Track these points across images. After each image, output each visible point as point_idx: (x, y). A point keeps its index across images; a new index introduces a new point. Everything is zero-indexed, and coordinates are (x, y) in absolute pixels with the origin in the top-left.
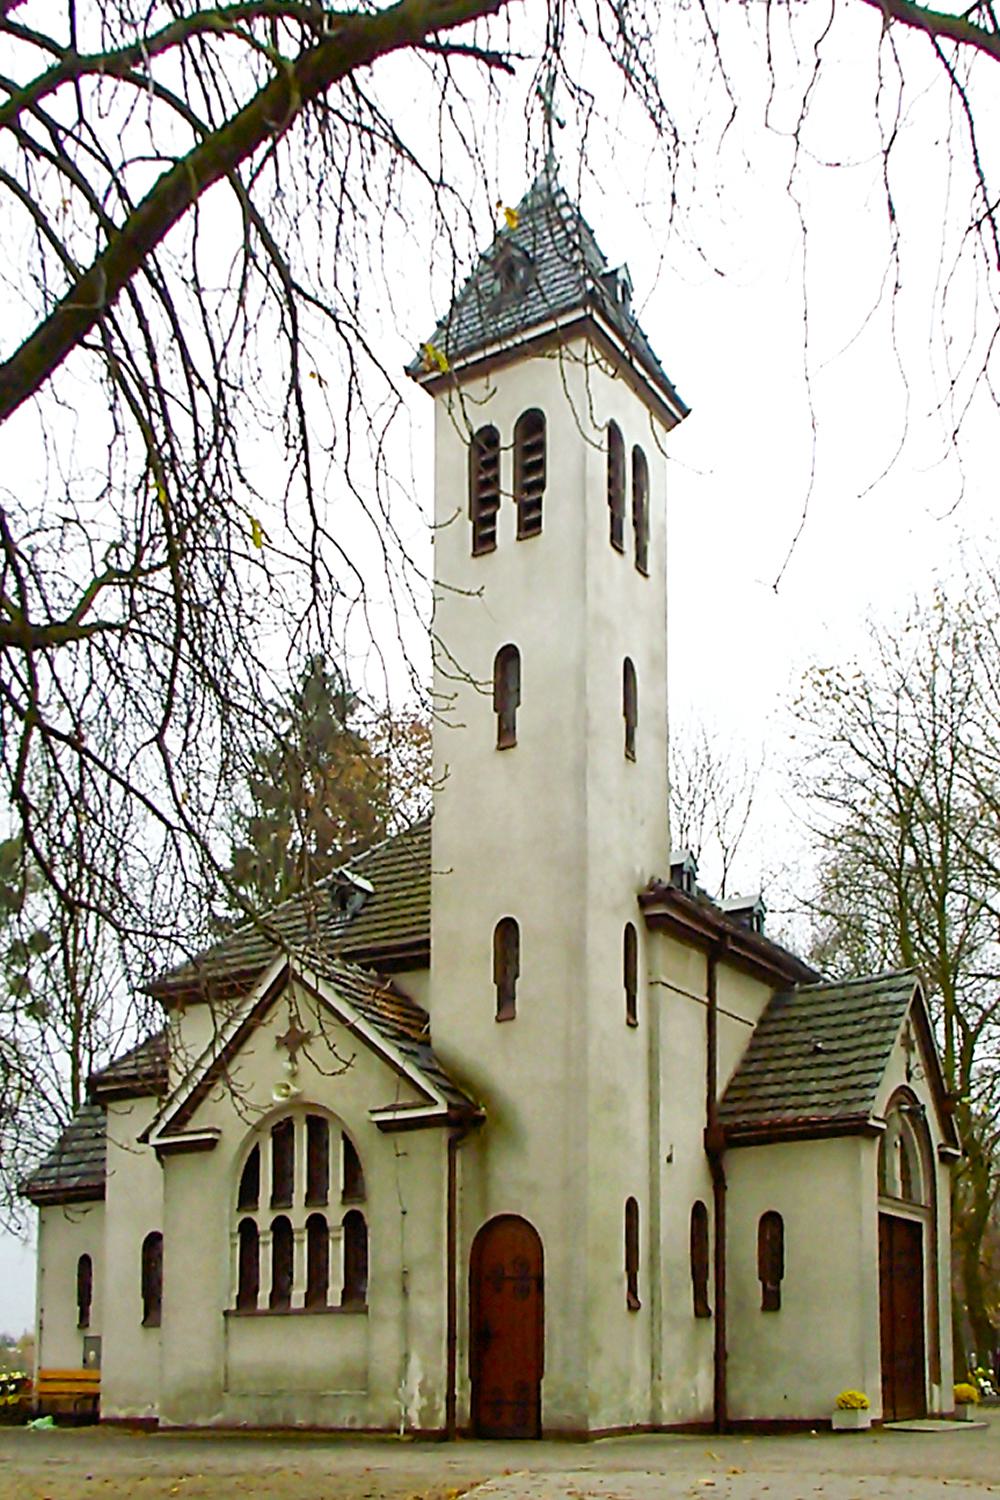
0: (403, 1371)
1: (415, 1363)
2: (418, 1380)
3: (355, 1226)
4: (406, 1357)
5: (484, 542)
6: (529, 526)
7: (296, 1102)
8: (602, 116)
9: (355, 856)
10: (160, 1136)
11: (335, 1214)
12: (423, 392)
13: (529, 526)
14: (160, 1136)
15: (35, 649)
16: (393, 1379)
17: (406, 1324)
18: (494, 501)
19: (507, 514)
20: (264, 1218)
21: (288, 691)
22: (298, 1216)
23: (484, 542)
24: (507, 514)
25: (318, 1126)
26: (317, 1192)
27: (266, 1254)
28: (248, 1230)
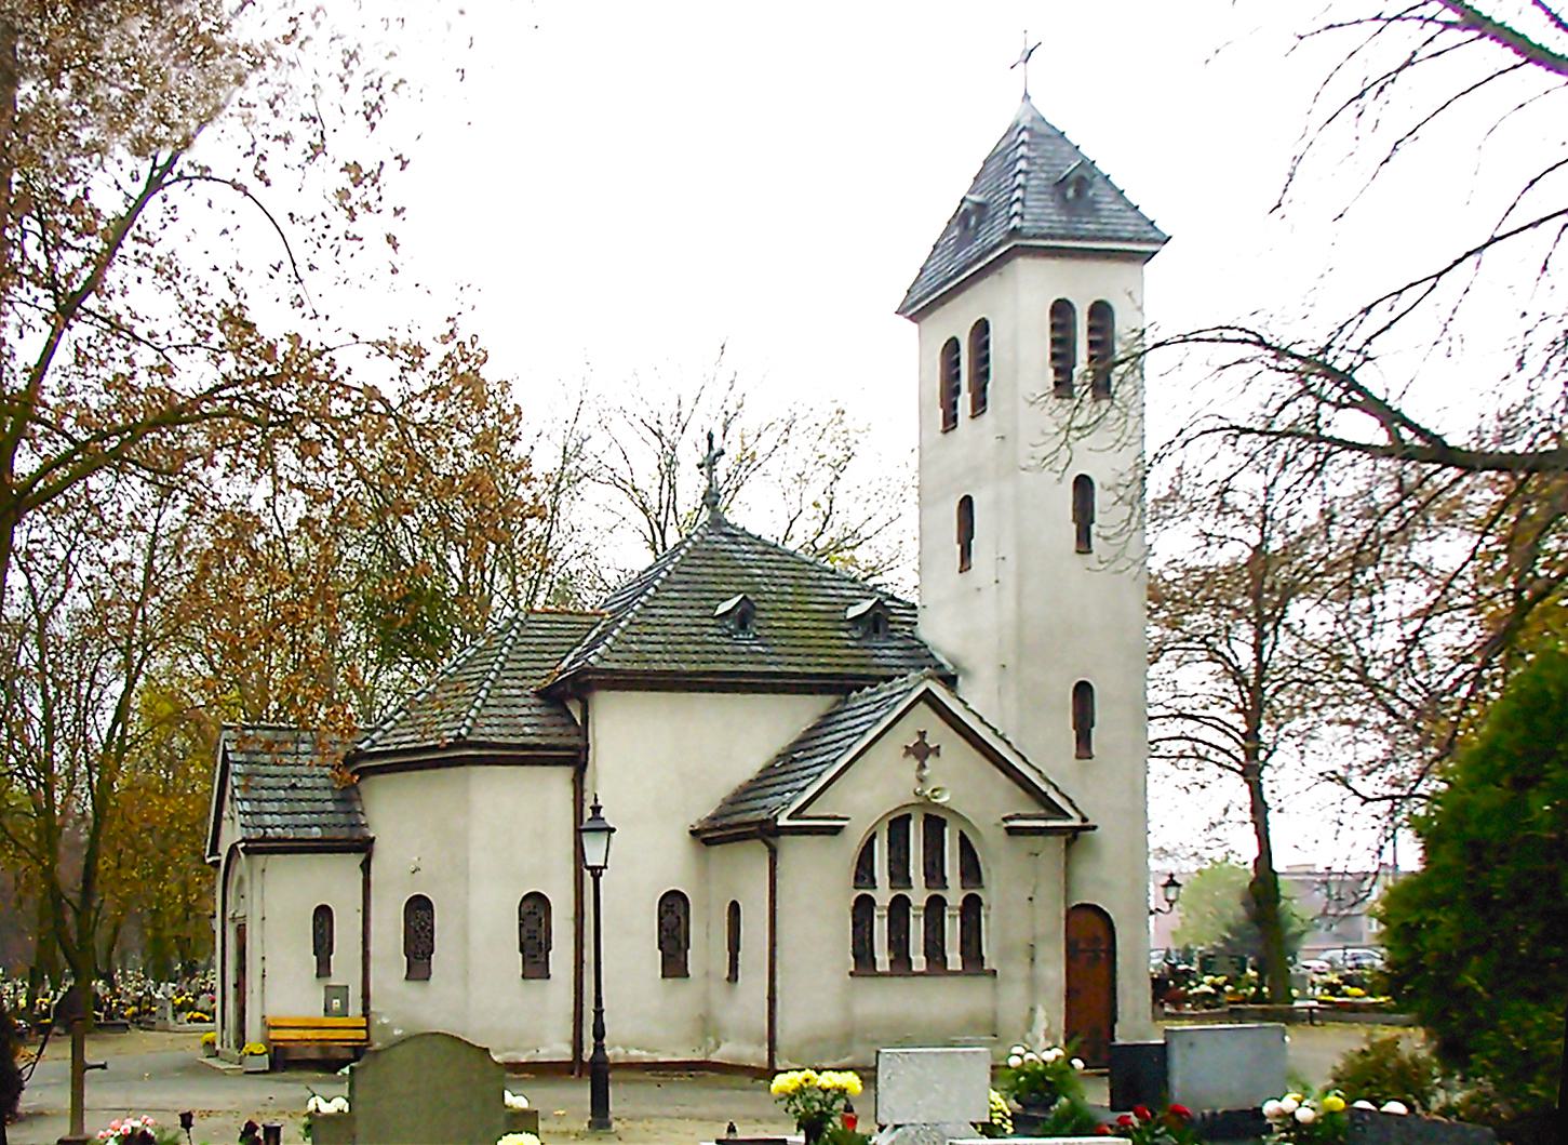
0: (1030, 1024)
1: (1041, 1014)
2: (1044, 1025)
3: (972, 907)
4: (1032, 1010)
5: (950, 421)
6: (979, 405)
7: (925, 803)
8: (1347, 863)
9: (1495, 656)
10: (789, 818)
11: (954, 896)
12: (908, 322)
13: (979, 405)
14: (789, 818)
15: (4, 230)
16: (1021, 1026)
17: (1033, 983)
18: (957, 391)
19: (964, 401)
20: (883, 895)
21: (403, 369)
22: (918, 895)
23: (950, 421)
24: (964, 401)
25: (935, 826)
26: (935, 874)
27: (881, 927)
28: (864, 907)
